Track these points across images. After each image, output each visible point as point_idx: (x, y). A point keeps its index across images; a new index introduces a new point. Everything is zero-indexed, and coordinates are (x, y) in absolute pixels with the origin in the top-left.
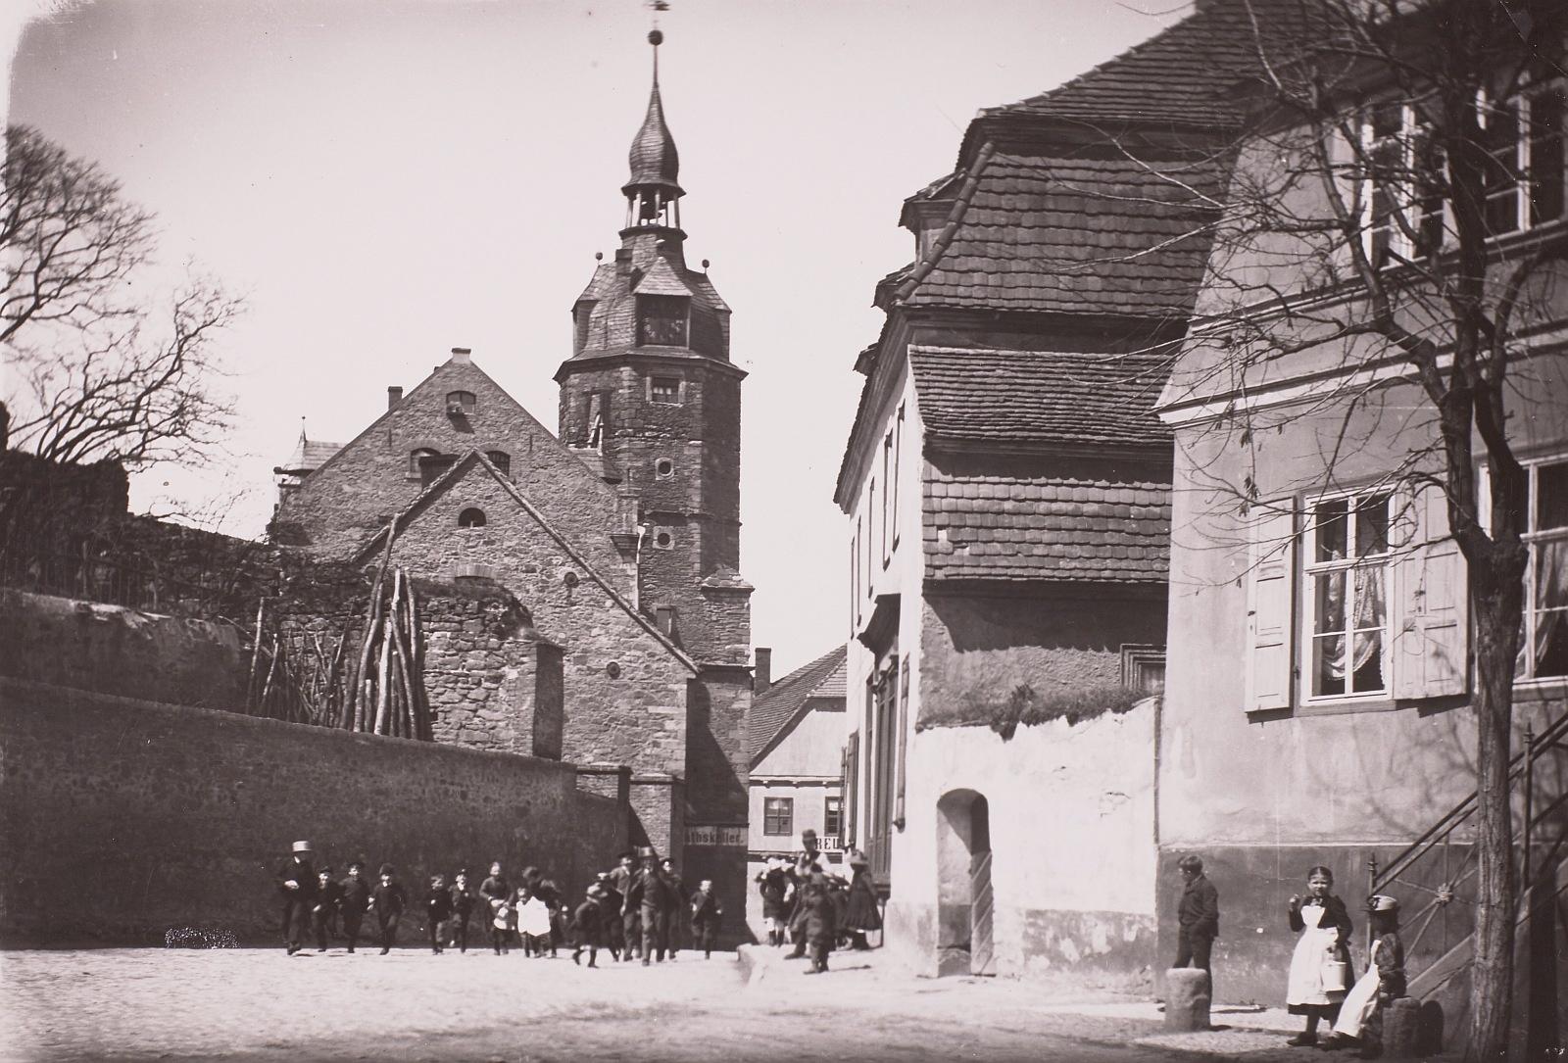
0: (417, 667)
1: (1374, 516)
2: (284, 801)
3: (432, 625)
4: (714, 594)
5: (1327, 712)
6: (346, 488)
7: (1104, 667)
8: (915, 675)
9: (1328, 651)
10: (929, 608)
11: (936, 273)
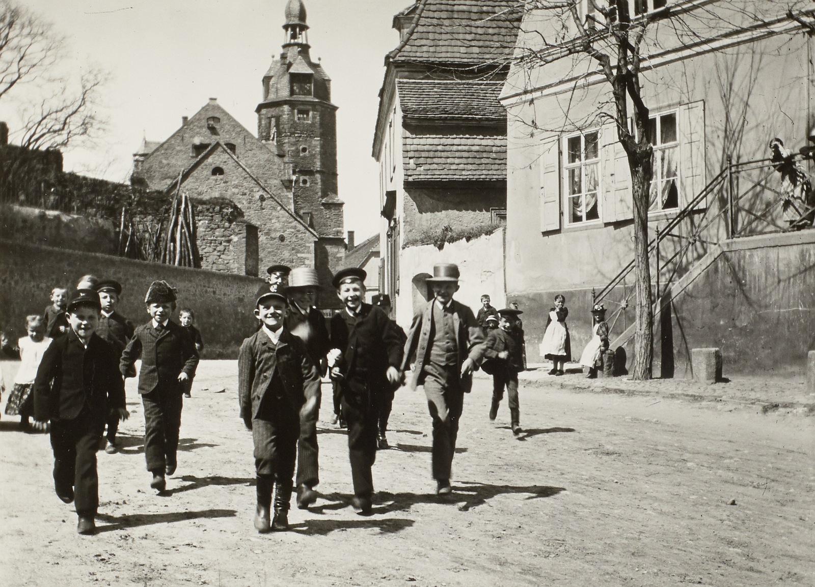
0: (193, 236)
1: (592, 139)
2: (132, 295)
3: (200, 218)
4: (328, 206)
5: (575, 230)
6: (164, 162)
7: (483, 217)
8: (402, 224)
9: (576, 204)
10: (407, 194)
11: (407, 46)
